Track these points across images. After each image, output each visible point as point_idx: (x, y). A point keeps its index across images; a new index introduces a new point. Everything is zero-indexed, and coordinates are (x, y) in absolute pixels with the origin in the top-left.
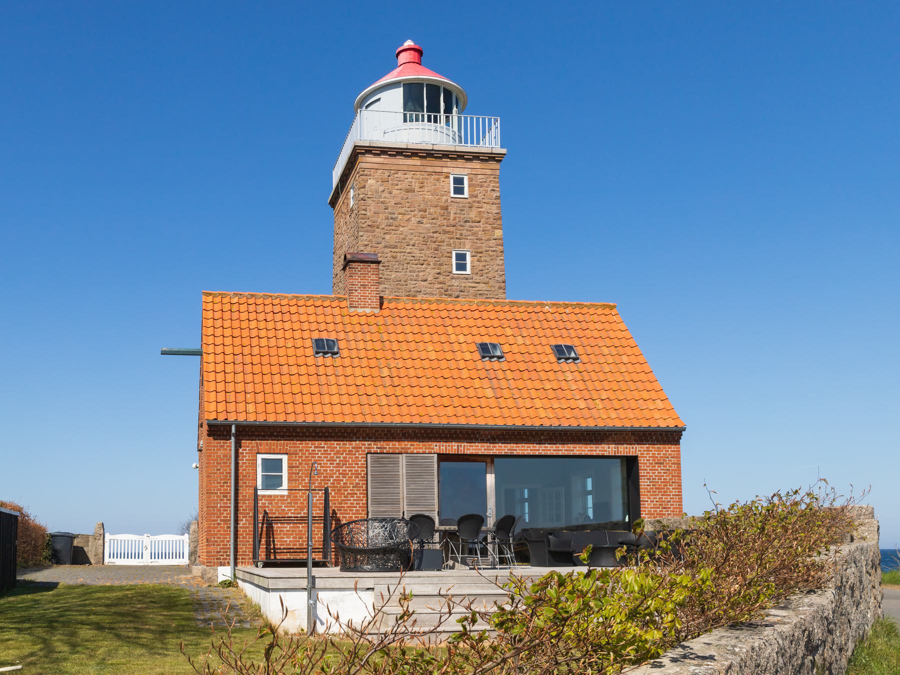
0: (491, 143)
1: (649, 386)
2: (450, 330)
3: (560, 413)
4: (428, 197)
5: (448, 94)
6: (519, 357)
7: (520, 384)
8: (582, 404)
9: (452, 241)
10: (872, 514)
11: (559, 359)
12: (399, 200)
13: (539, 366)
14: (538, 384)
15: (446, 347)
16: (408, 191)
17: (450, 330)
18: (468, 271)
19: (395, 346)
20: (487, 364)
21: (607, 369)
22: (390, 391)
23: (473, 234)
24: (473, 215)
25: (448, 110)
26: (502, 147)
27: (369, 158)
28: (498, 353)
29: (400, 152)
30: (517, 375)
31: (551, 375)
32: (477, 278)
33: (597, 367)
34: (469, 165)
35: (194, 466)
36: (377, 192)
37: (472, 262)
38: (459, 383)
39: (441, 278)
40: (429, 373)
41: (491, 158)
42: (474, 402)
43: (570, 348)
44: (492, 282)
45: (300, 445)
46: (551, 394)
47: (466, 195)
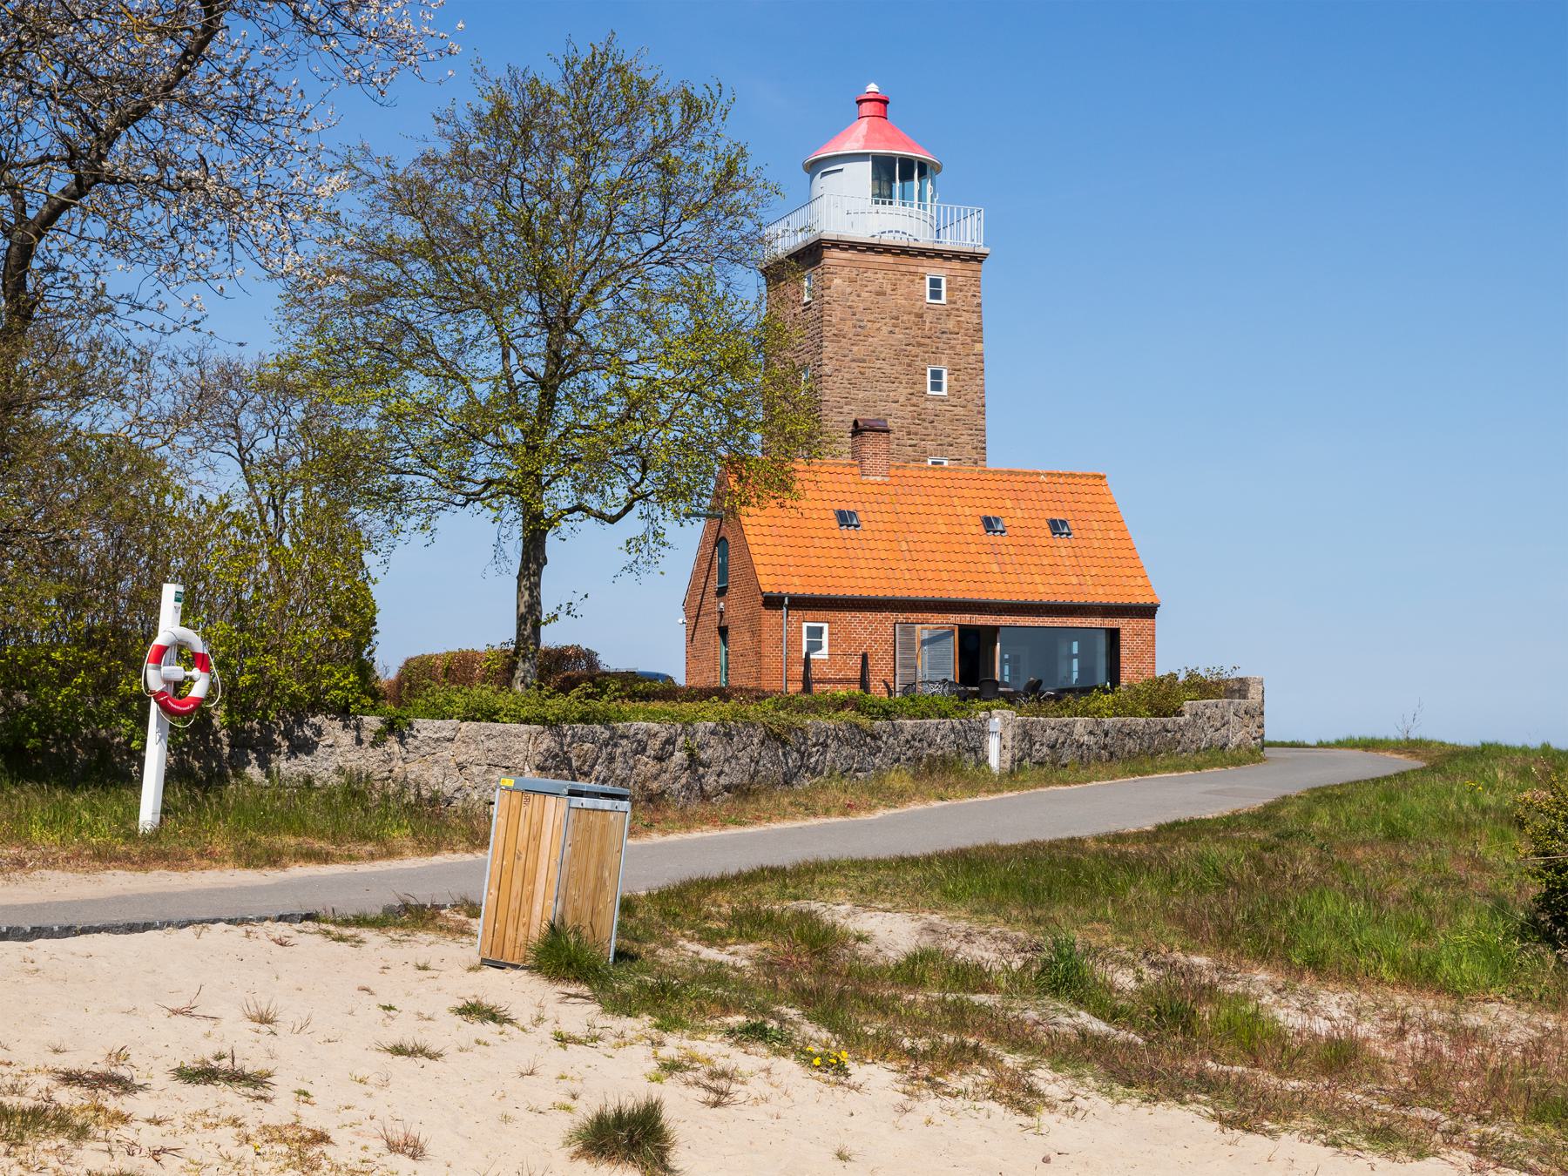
0: (967, 235)
6: (1019, 532)
7: (1021, 559)
8: (1074, 580)
10: (1261, 683)
12: (868, 304)
13: (1037, 542)
14: (1036, 560)
16: (878, 294)
18: (944, 392)
19: (909, 518)
20: (990, 537)
21: (1096, 545)
22: (910, 565)
23: (952, 348)
24: (951, 324)
27: (836, 253)
29: (871, 248)
32: (954, 400)
34: (948, 264)
39: (914, 400)
40: (942, 547)
41: (976, 258)
42: (983, 577)
43: (1064, 523)
44: (970, 406)
46: (1048, 570)
47: (944, 300)
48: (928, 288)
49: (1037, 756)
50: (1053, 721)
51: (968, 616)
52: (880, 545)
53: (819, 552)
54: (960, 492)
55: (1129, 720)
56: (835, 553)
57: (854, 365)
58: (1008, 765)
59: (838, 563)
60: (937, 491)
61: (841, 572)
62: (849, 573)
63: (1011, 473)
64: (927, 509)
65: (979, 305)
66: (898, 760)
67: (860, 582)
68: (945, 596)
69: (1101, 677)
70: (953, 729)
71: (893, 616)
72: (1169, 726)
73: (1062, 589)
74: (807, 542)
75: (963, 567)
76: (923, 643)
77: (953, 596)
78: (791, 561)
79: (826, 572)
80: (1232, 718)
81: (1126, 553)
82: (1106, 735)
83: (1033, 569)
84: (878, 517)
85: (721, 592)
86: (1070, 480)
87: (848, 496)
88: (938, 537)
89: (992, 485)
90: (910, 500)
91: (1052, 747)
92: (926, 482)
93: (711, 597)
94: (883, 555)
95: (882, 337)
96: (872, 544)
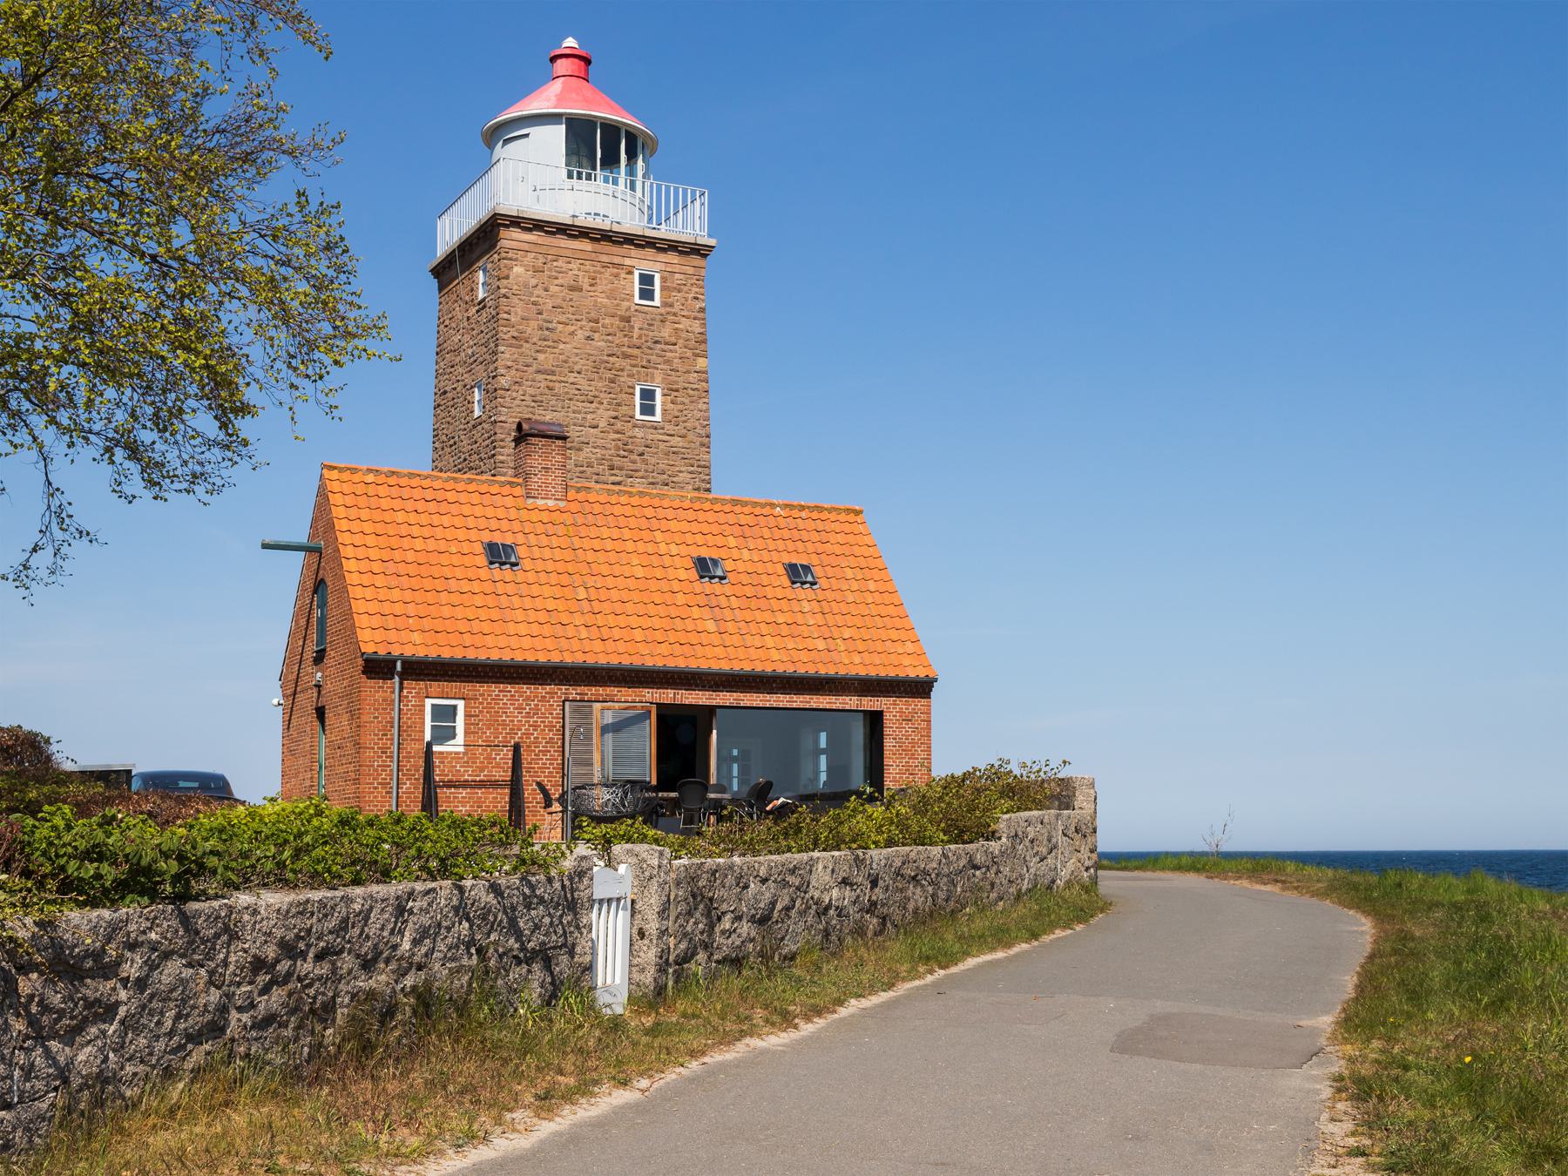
0: (691, 225)
1: (898, 623)
2: (659, 536)
3: (795, 655)
4: (603, 300)
5: (632, 138)
6: (745, 579)
7: (748, 615)
8: (821, 644)
9: (635, 370)
10: (1092, 785)
11: (794, 583)
12: (559, 302)
13: (769, 592)
14: (768, 616)
15: (655, 560)
16: (572, 289)
17: (659, 536)
18: (658, 417)
19: (590, 556)
20: (707, 586)
22: (589, 619)
23: (667, 362)
24: (666, 333)
25: (632, 156)
26: (710, 236)
27: (515, 233)
28: (719, 573)
29: (562, 229)
30: (742, 603)
31: (784, 605)
32: (670, 428)
33: (837, 596)
34: (662, 257)
35: (275, 701)
36: (526, 285)
37: (664, 403)
38: (673, 612)
39: (619, 425)
40: (636, 596)
41: (697, 250)
42: (693, 638)
43: (807, 568)
44: (691, 436)
45: (482, 688)
46: (785, 630)
47: (657, 302)
48: (637, 286)
49: (725, 946)
50: (766, 861)
51: (671, 693)
52: (547, 591)
53: (455, 599)
54: (664, 525)
55: (913, 851)
56: (478, 600)
57: (540, 377)
58: (648, 978)
59: (483, 614)
60: (633, 523)
61: (486, 627)
62: (497, 628)
63: (735, 502)
64: (618, 546)
65: (702, 310)
66: (215, 1029)
67: (514, 642)
69: (858, 780)
70: (461, 911)
71: (562, 690)
72: (979, 858)
73: (804, 656)
74: (439, 584)
75: (666, 623)
76: (605, 729)
77: (649, 663)
78: (411, 609)
79: (462, 626)
80: (1059, 838)
81: (891, 610)
82: (874, 883)
83: (764, 629)
84: (547, 553)
85: (319, 658)
86: (815, 515)
87: (505, 525)
88: (631, 583)
89: (711, 517)
90: (593, 532)
91: (763, 920)
92: (617, 510)
93: (308, 667)
94: (551, 604)
95: (575, 344)
96: (535, 590)
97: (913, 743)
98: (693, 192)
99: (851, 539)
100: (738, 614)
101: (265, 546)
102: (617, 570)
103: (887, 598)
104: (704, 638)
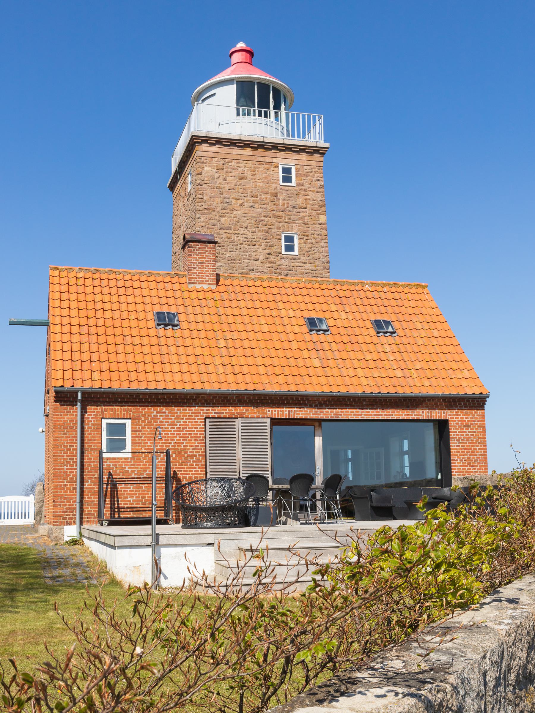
0: (316, 137)
1: (457, 357)
3: (380, 381)
4: (260, 184)
5: (277, 92)
6: (342, 331)
7: (344, 355)
8: (399, 373)
9: (281, 225)
11: (378, 333)
12: (233, 186)
13: (360, 339)
14: (360, 356)
15: (277, 321)
18: (296, 252)
19: (231, 319)
20: (314, 336)
23: (300, 219)
24: (300, 201)
25: (277, 107)
26: (325, 141)
27: (206, 147)
28: (324, 327)
29: (233, 143)
30: (341, 346)
31: (371, 347)
32: (304, 259)
34: (296, 156)
35: (40, 430)
36: (212, 178)
38: (289, 354)
39: (272, 258)
40: (262, 344)
41: (316, 151)
43: (388, 323)
44: (317, 263)
46: (372, 364)
47: (294, 183)
68: (259, 388)
71: (204, 410)
73: (387, 382)
77: (268, 389)
83: (356, 364)
97: (472, 443)
98: (314, 117)
99: (420, 303)
100: (337, 355)
101: (11, 323)
102: (249, 327)
103: (447, 341)
104: (311, 371)
